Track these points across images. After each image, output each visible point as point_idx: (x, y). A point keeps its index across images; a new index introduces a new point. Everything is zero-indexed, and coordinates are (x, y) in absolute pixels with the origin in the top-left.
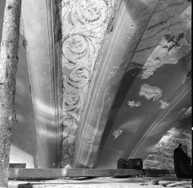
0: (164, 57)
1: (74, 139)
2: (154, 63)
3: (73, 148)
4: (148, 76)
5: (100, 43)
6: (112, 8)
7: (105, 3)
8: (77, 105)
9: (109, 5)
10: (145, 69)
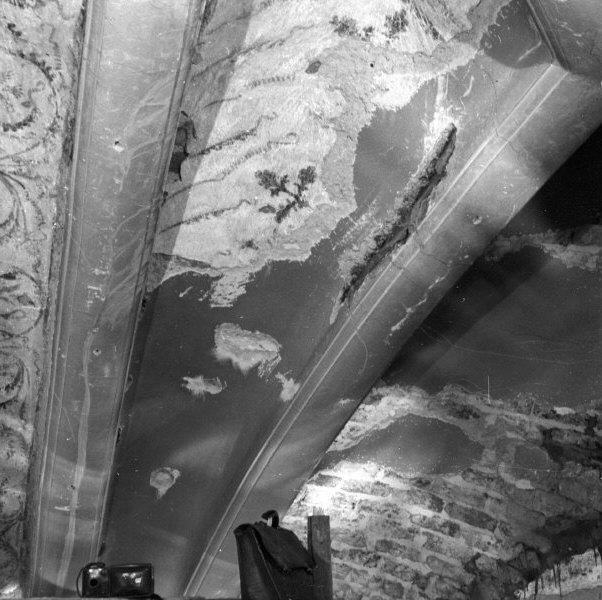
0: (269, 241)
1: (23, 499)
2: (240, 257)
3: (21, 528)
4: (232, 297)
5: (52, 196)
6: (65, 87)
7: (43, 74)
8: (16, 389)
9: (57, 80)
10: (218, 278)
